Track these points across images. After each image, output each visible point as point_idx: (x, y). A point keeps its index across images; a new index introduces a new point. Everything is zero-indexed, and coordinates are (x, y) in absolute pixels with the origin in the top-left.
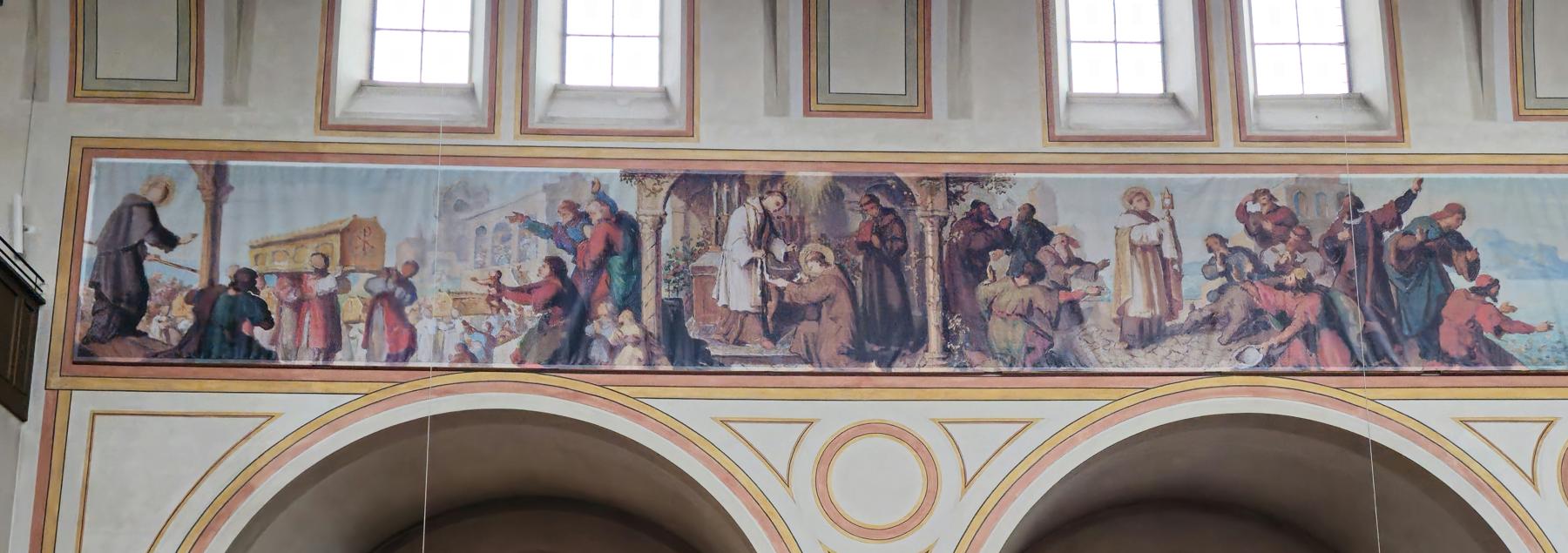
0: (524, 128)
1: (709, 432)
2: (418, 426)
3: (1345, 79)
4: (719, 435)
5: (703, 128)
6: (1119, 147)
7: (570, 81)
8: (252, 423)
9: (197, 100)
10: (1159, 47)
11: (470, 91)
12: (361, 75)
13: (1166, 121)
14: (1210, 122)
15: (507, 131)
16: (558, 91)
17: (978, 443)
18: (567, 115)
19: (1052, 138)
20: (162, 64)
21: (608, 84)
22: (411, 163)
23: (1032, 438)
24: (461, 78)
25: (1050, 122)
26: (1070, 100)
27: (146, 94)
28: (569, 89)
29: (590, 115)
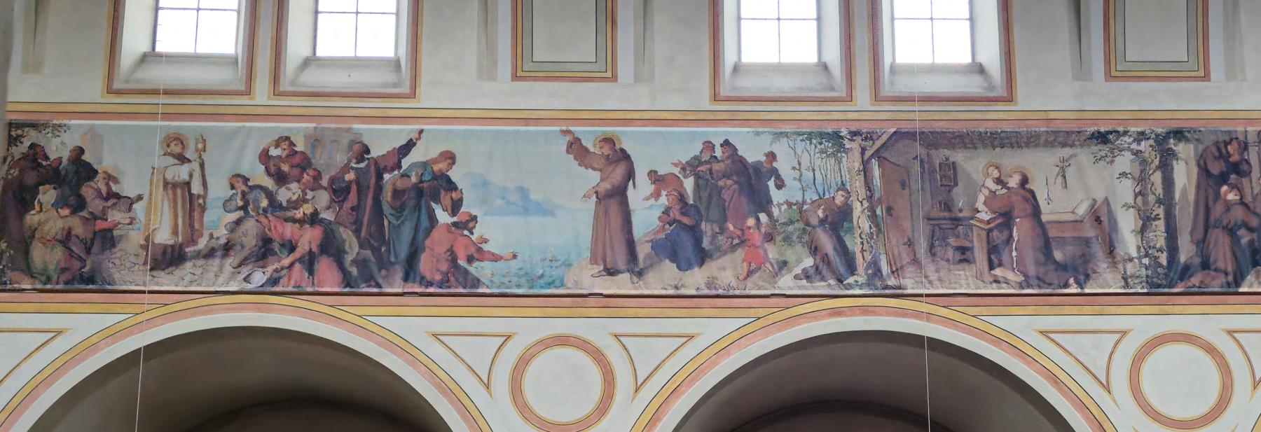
1: (1032, 339)
3: (159, 28)
5: (1020, 92)
7: (319, 53)
9: (1206, 77)
10: (968, 23)
11: (396, 64)
13: (973, 86)
15: (262, 95)
16: (310, 61)
17: (1094, 351)
19: (110, 91)
21: (352, 54)
22: (735, 126)
23: (60, 346)
24: (388, 51)
25: (110, 76)
26: (736, 69)
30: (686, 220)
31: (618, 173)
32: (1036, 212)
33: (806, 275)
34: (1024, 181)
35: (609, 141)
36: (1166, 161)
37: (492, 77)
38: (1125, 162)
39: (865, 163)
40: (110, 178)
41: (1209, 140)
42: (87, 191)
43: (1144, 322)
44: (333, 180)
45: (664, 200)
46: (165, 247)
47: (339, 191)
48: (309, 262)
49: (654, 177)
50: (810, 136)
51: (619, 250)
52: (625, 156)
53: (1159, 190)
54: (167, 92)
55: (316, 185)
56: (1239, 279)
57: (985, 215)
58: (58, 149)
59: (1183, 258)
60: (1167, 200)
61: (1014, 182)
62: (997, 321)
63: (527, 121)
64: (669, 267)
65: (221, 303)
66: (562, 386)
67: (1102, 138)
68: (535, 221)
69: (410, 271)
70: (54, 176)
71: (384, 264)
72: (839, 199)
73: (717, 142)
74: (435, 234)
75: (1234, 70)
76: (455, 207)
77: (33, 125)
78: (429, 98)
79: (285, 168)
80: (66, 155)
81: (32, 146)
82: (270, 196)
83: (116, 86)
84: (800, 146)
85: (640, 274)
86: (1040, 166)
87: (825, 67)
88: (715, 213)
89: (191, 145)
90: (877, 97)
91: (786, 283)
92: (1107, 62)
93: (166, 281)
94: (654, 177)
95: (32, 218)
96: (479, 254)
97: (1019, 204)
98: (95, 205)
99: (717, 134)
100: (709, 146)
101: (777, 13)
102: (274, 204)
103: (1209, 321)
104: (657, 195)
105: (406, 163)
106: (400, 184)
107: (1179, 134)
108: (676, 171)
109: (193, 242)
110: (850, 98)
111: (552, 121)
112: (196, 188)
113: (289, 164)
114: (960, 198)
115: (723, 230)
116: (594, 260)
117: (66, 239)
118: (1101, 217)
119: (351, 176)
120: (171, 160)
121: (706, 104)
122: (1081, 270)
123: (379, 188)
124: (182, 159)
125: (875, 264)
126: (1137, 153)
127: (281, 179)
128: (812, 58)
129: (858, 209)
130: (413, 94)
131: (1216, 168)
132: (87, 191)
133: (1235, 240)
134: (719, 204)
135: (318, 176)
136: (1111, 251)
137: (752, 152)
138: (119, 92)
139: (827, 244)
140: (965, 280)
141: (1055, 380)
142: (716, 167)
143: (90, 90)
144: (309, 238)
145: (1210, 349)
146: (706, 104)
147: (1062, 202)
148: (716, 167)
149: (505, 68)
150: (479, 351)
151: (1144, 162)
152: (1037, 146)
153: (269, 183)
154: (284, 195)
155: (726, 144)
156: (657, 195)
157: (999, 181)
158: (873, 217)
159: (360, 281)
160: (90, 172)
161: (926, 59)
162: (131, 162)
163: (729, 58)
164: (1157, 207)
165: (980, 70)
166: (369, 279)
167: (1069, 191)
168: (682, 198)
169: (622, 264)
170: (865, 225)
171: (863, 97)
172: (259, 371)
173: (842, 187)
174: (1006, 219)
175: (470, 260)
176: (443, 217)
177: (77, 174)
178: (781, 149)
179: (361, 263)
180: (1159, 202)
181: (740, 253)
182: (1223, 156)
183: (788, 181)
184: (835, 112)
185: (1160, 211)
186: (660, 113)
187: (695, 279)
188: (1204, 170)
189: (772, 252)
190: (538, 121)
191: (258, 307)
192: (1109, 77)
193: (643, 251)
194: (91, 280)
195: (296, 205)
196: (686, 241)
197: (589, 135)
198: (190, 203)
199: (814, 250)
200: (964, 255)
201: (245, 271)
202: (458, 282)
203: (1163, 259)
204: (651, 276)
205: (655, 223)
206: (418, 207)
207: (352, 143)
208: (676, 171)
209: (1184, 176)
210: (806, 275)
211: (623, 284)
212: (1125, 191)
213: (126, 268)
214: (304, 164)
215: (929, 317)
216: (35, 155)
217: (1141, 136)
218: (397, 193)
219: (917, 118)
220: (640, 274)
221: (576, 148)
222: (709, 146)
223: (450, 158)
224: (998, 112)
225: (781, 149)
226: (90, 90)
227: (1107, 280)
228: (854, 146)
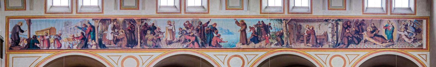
2: (62, 58)
4: (107, 58)
5: (104, 12)
7: (54, 5)
9: (345, 10)
12: (293, 5)
13: (174, 10)
14: (181, 10)
15: (183, 13)
16: (82, 6)
17: (324, 58)
19: (157, 13)
23: (257, 57)
25: (157, 10)
26: (394, 9)
29: (273, 10)
30: (256, 35)
31: (244, 27)
32: (315, 34)
33: (276, 45)
34: (313, 28)
35: (242, 21)
36: (337, 24)
37: (117, 9)
38: (330, 25)
39: (286, 25)
40: (159, 29)
41: (344, 21)
42: (155, 31)
43: (332, 53)
44: (197, 28)
45: (252, 32)
46: (169, 41)
47: (198, 30)
48: (193, 43)
49: (250, 27)
50: (276, 20)
51: (244, 40)
52: (245, 24)
53: (336, 30)
54: (269, 13)
55: (193, 29)
56: (348, 45)
57: (306, 34)
58: (150, 24)
59: (339, 42)
60: (337, 32)
61: (311, 28)
62: (308, 52)
63: (228, 17)
64: (253, 43)
65: (178, 50)
66: (236, 63)
67: (326, 21)
68: (230, 35)
69: (210, 45)
70: (150, 29)
71: (206, 43)
72: (281, 31)
73: (261, 21)
74: (214, 38)
76: (217, 33)
77: (145, 19)
78: (211, 13)
79: (188, 26)
80: (151, 25)
81: (145, 23)
82: (186, 31)
83: (262, 12)
84: (275, 22)
85: (248, 45)
86: (316, 25)
87: (382, 8)
88: (260, 34)
89: (172, 22)
90: (289, 13)
91: (273, 46)
92: (328, 6)
93: (169, 47)
94: (250, 27)
95: (146, 36)
96: (221, 41)
97: (312, 32)
98: (157, 34)
99: (261, 20)
100: (259, 22)
102: (187, 33)
103: (343, 53)
104: (251, 31)
105: (208, 25)
106: (208, 29)
107: (339, 20)
108: (254, 26)
109: (174, 40)
110: (284, 13)
111: (233, 17)
112: (174, 30)
113: (189, 26)
114: (302, 31)
115: (262, 37)
116: (240, 42)
117: (153, 40)
118: (326, 35)
119: (199, 28)
120: (169, 25)
121: (259, 14)
122: (321, 44)
123: (204, 30)
124: (171, 25)
125: (287, 43)
126: (332, 23)
127: (187, 28)
128: (380, 6)
129: (284, 33)
130: (208, 13)
131: (346, 26)
132: (155, 31)
133: (348, 39)
134: (261, 33)
135: (194, 28)
136: (327, 40)
137: (267, 23)
138: (159, 13)
139: (279, 39)
140: (302, 45)
141: (317, 62)
142: (260, 26)
143: (154, 13)
144: (193, 39)
145: (343, 58)
146: (259, 14)
147: (319, 32)
148: (260, 26)
150: (222, 58)
151: (333, 25)
152: (357, 22)
153: (185, 29)
154: (188, 31)
155: (262, 21)
156: (251, 31)
157: (308, 28)
158: (287, 35)
159: (203, 46)
160: (155, 28)
162: (162, 26)
163: (366, 6)
164: (335, 33)
165: (410, 9)
166: (203, 45)
167: (321, 30)
168: (255, 31)
169: (245, 43)
170: (286, 36)
173: (282, 29)
174: (309, 35)
175: (220, 42)
176: (215, 35)
177: (153, 28)
178: (272, 22)
179: (202, 43)
180: (336, 32)
181: (265, 41)
182: (347, 24)
183: (273, 28)
184: (281, 15)
185: (336, 34)
186: (251, 16)
187: (257, 45)
188: (343, 27)
189: (270, 41)
190: (230, 17)
191: (185, 51)
192: (329, 9)
193: (249, 40)
194: (157, 47)
195: (190, 33)
196: (256, 39)
197: (239, 20)
198: (173, 33)
199: (277, 40)
200: (302, 41)
201: (183, 45)
202: (218, 46)
203: (336, 42)
204: (250, 45)
205: (251, 36)
206: (211, 33)
207: (199, 22)
208: (254, 26)
209: (340, 27)
210: (276, 45)
211: (245, 46)
212: (330, 30)
213: (163, 44)
214: (191, 26)
215: (296, 52)
216: (146, 25)
217: (333, 20)
218: (207, 31)
219: (295, 16)
220: (248, 45)
221: (237, 22)
222: (259, 22)
223: (216, 24)
224: (309, 15)
225: (272, 22)
226: (154, 13)
227: (326, 46)
228: (284, 22)
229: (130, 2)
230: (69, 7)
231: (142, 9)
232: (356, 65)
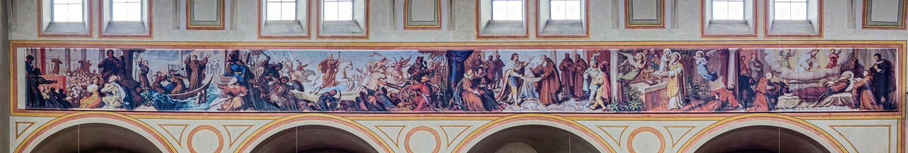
0: (538, 36)
5: (371, 34)
6: (516, 37)
8: (688, 129)
9: (440, 28)
11: (746, 23)
13: (743, 30)
14: (756, 30)
15: (313, 39)
17: (176, 131)
18: (495, 31)
20: (430, 17)
21: (336, 19)
23: (695, 131)
25: (703, 32)
26: (110, 24)
27: (648, 25)
28: (553, 21)
29: (506, 31)
37: (178, 28)
75: (452, 26)
92: (626, 20)
101: (281, 3)
141: (161, 141)
149: (183, 23)
150: (616, 133)
161: (278, 19)
163: (708, 18)
165: (746, 23)
171: (761, 35)
172: (114, 141)
192: (627, 27)
229: (644, 11)
230: (581, 23)
231: (449, 28)
232: (244, 147)
